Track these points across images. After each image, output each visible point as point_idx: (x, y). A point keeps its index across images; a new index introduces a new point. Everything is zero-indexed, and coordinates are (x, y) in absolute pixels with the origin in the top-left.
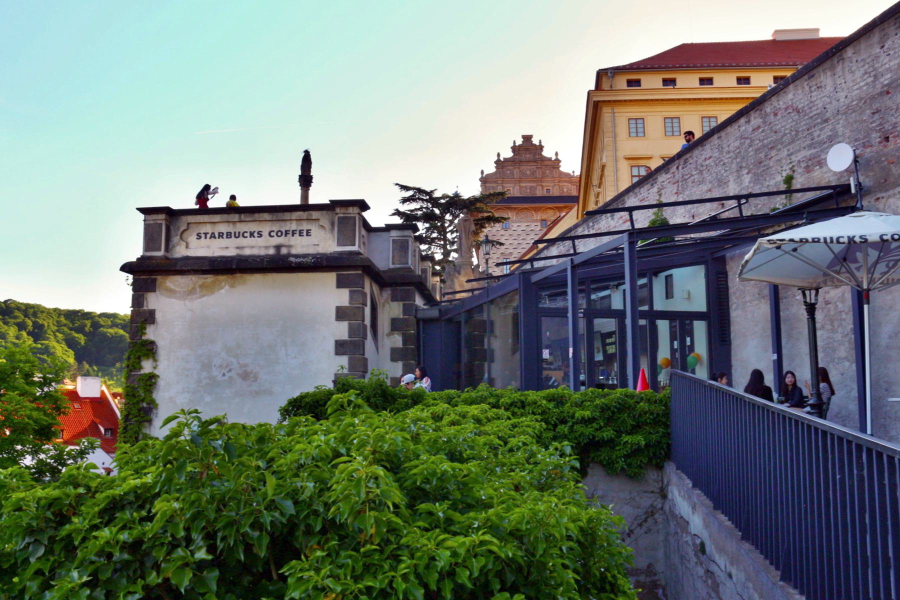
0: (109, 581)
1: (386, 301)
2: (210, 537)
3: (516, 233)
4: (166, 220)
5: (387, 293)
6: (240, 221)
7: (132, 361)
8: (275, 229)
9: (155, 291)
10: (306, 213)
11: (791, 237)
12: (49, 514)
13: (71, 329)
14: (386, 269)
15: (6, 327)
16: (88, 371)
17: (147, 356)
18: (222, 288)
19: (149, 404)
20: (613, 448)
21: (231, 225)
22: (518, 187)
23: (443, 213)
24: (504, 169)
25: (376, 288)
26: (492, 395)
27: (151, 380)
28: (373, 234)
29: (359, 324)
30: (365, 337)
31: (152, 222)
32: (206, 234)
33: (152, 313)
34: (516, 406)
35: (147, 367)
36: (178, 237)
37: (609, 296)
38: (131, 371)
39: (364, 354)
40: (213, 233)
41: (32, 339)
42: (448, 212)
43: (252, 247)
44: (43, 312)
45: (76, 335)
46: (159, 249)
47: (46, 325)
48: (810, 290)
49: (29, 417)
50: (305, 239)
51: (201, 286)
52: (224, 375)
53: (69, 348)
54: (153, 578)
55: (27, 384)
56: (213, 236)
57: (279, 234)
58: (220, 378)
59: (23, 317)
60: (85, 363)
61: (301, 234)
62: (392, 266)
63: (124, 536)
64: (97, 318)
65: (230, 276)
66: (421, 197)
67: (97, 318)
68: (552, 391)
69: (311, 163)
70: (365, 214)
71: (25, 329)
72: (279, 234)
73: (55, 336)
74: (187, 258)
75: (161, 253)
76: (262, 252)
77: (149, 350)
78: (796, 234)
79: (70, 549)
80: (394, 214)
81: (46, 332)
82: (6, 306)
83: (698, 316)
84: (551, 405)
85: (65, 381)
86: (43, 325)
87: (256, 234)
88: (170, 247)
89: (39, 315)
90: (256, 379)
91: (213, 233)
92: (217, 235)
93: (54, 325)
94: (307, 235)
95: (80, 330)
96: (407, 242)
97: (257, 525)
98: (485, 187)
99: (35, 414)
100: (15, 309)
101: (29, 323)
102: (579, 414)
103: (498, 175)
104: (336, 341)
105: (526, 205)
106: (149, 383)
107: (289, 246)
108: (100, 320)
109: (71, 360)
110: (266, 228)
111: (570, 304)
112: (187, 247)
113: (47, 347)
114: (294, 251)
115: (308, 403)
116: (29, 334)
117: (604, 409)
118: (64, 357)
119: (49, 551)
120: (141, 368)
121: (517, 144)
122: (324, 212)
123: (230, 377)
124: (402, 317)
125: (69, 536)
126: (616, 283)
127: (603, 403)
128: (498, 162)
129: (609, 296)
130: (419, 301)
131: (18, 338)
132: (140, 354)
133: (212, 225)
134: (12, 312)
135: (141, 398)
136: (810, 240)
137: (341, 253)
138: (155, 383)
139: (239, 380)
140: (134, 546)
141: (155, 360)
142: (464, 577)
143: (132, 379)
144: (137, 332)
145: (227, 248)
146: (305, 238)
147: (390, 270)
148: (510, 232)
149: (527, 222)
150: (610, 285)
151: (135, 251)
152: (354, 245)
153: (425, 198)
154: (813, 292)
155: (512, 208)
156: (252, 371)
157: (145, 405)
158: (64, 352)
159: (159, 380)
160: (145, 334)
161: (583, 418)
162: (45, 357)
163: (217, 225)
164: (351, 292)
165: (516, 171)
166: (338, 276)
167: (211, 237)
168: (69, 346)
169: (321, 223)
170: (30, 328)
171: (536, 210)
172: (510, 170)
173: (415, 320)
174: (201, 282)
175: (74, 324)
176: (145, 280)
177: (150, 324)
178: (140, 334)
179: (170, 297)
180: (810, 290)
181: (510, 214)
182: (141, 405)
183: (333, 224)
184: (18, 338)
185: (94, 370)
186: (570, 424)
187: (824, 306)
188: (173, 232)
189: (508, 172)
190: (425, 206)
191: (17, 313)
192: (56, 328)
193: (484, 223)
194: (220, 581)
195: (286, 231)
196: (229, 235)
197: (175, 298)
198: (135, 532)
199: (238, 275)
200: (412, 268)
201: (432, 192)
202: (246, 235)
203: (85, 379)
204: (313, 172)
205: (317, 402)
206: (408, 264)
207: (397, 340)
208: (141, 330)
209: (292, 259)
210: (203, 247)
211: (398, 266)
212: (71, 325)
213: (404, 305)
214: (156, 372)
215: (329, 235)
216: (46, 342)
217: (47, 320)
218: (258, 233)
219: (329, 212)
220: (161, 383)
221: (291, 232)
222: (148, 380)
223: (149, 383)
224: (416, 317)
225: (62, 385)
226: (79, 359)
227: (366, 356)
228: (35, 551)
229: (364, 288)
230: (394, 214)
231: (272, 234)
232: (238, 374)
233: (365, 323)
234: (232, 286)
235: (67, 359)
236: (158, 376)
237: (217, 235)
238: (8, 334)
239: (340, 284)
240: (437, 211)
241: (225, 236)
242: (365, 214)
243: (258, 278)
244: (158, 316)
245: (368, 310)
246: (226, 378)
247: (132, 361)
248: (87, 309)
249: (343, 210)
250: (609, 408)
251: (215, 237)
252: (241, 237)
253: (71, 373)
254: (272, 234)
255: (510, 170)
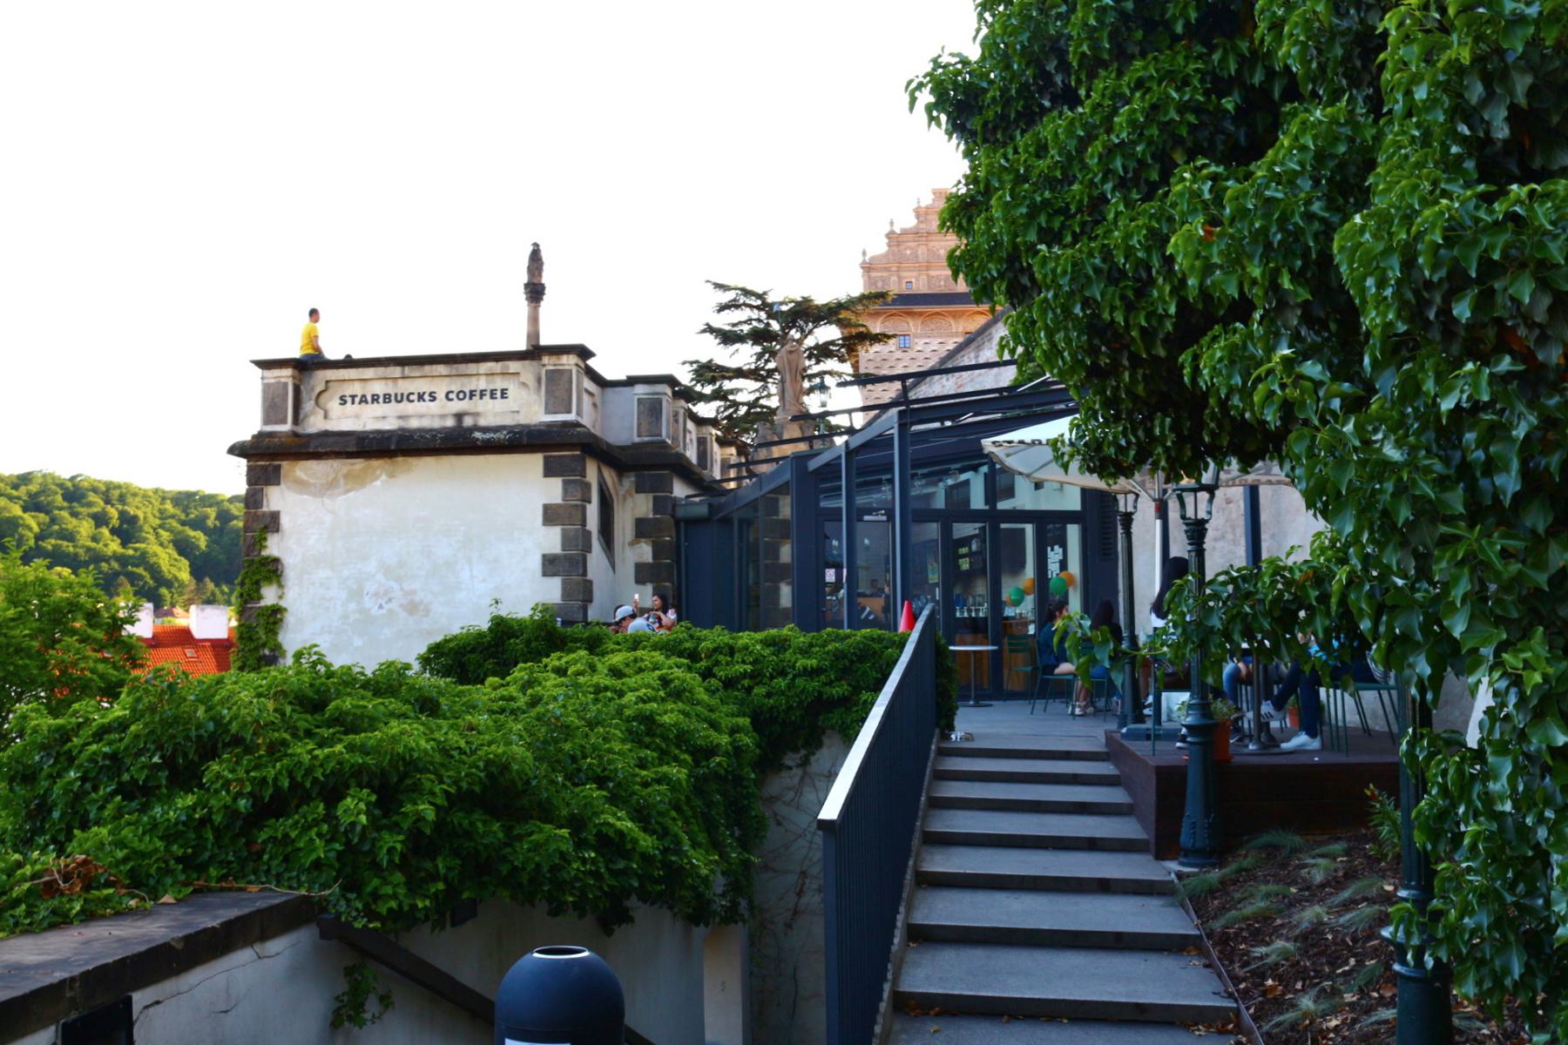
0: (95, 778)
1: (628, 493)
2: (160, 747)
3: (922, 356)
4: (294, 377)
5: (629, 481)
6: (404, 378)
7: (246, 587)
8: (456, 388)
9: (279, 484)
10: (500, 364)
11: (1021, 438)
12: (57, 736)
13: (183, 524)
14: (629, 443)
15: (74, 521)
16: (213, 594)
17: (269, 580)
18: (377, 478)
19: (272, 650)
20: (849, 709)
21: (390, 383)
22: (925, 277)
23: (786, 327)
24: (902, 247)
25: (609, 475)
26: (691, 637)
27: (275, 615)
28: (609, 391)
29: (577, 530)
30: (588, 548)
31: (272, 381)
32: (353, 397)
33: (275, 516)
34: (721, 653)
35: (269, 596)
36: (313, 402)
37: (967, 482)
38: (246, 602)
39: (585, 573)
40: (364, 396)
41: (119, 541)
42: (794, 326)
43: (421, 416)
44: (135, 495)
45: (192, 533)
46: (284, 421)
47: (141, 515)
48: (1126, 494)
49: (93, 671)
50: (499, 404)
51: (346, 476)
52: (381, 607)
53: (180, 554)
54: (126, 777)
55: (90, 626)
56: (363, 400)
57: (461, 395)
58: (375, 611)
59: (102, 503)
60: (207, 580)
61: (493, 396)
62: (637, 440)
63: (106, 749)
64: (226, 504)
65: (388, 461)
66: (748, 301)
67: (226, 504)
68: (773, 632)
69: (542, 264)
70: (591, 362)
71: (107, 524)
72: (461, 396)
73: (157, 535)
74: (326, 434)
75: (286, 427)
76: (437, 424)
77: (272, 570)
78: (1016, 436)
79: (71, 760)
80: (704, 331)
81: (141, 529)
82: (74, 486)
83: (1069, 517)
84: (767, 652)
85: (175, 610)
86: (135, 518)
87: (426, 397)
88: (301, 417)
89: (130, 499)
90: (427, 611)
91: (364, 396)
92: (369, 399)
93: (154, 516)
94: (502, 397)
95: (198, 524)
96: (660, 402)
97: (188, 738)
98: (869, 278)
99: (101, 667)
100: (88, 490)
101: (113, 513)
102: (802, 662)
103: (891, 258)
104: (544, 556)
105: (937, 309)
106: (271, 620)
107: (476, 415)
108: (232, 507)
109: (185, 575)
110: (441, 388)
111: (844, 505)
112: (326, 417)
113: (144, 554)
114: (483, 422)
115: (451, 649)
116: (113, 531)
117: (838, 656)
118: (174, 571)
119: (57, 760)
120: (260, 598)
121: (923, 204)
122: (527, 362)
123: (390, 611)
124: (651, 516)
125: (70, 751)
126: (958, 466)
127: (836, 649)
128: (891, 236)
129: (967, 482)
130: (680, 490)
131: (95, 539)
132: (258, 577)
133: (362, 383)
134: (83, 496)
135: (261, 642)
136: (1044, 442)
137: (550, 425)
138: (281, 620)
139: (403, 615)
140: (113, 757)
141: (281, 586)
142: (319, 774)
143: (247, 614)
144: (254, 545)
145: (384, 418)
146: (499, 401)
147: (635, 446)
148: (911, 354)
149: (941, 337)
150: (950, 469)
151: (250, 425)
152: (569, 411)
153: (755, 304)
154: (1131, 497)
155: (915, 313)
156: (422, 601)
157: (267, 652)
158: (173, 562)
159: (286, 614)
160: (265, 547)
161: (805, 669)
162: (140, 571)
163: (369, 383)
164: (565, 483)
165: (922, 251)
166: (545, 458)
167: (360, 402)
168: (181, 553)
169: (523, 378)
170: (115, 522)
171: (955, 315)
172: (911, 249)
173: (672, 521)
174: (345, 470)
175: (187, 515)
176: (264, 468)
177: (273, 532)
178: (258, 547)
179: (301, 493)
180: (1126, 494)
181: (911, 324)
182: (261, 653)
183: (539, 380)
184: (95, 539)
185: (223, 593)
186: (790, 676)
187: (1224, 505)
188: (304, 394)
189: (908, 252)
190: (755, 317)
191: (92, 497)
192: (158, 522)
193: (855, 344)
194: (168, 779)
195: (471, 392)
196: (387, 398)
197: (309, 493)
198: (114, 747)
199: (400, 459)
200: (669, 442)
201: (765, 293)
202: (412, 397)
203: (203, 610)
204: (546, 279)
205: (464, 647)
206: (660, 435)
207: (645, 552)
208: (260, 542)
209: (478, 435)
210: (348, 417)
211: (646, 439)
212: (183, 517)
213: (655, 499)
214: (283, 604)
215: (534, 397)
216: (142, 546)
217: (143, 509)
218: (430, 395)
219: (535, 363)
220: (290, 619)
221: (478, 393)
222: (270, 615)
223: (271, 620)
224: (673, 516)
225: (170, 618)
226: (197, 573)
227: (590, 576)
228: (48, 760)
229: (584, 476)
230: (704, 331)
231: (451, 396)
232: (402, 606)
233: (588, 528)
234: (391, 476)
235: (177, 574)
236: (285, 610)
237: (369, 399)
238: (78, 532)
239: (549, 471)
240: (775, 326)
241: (381, 400)
242: (591, 362)
243: (428, 462)
244: (285, 521)
245: (593, 511)
246: (383, 611)
247: (246, 587)
248: (208, 490)
249: (554, 360)
250: (845, 657)
251: (366, 402)
252: (405, 401)
253: (186, 597)
254: (451, 396)
255: (911, 249)
